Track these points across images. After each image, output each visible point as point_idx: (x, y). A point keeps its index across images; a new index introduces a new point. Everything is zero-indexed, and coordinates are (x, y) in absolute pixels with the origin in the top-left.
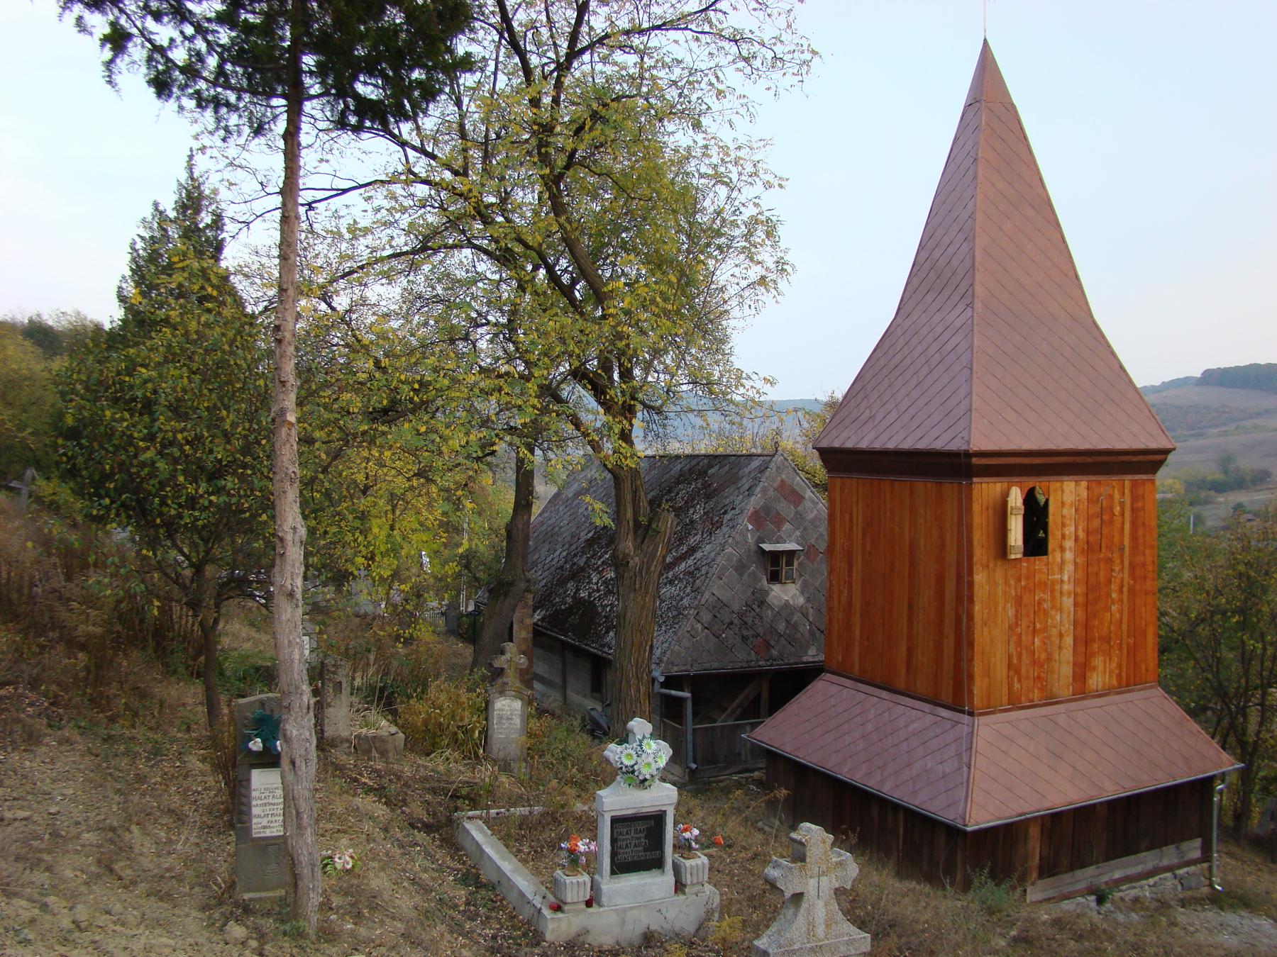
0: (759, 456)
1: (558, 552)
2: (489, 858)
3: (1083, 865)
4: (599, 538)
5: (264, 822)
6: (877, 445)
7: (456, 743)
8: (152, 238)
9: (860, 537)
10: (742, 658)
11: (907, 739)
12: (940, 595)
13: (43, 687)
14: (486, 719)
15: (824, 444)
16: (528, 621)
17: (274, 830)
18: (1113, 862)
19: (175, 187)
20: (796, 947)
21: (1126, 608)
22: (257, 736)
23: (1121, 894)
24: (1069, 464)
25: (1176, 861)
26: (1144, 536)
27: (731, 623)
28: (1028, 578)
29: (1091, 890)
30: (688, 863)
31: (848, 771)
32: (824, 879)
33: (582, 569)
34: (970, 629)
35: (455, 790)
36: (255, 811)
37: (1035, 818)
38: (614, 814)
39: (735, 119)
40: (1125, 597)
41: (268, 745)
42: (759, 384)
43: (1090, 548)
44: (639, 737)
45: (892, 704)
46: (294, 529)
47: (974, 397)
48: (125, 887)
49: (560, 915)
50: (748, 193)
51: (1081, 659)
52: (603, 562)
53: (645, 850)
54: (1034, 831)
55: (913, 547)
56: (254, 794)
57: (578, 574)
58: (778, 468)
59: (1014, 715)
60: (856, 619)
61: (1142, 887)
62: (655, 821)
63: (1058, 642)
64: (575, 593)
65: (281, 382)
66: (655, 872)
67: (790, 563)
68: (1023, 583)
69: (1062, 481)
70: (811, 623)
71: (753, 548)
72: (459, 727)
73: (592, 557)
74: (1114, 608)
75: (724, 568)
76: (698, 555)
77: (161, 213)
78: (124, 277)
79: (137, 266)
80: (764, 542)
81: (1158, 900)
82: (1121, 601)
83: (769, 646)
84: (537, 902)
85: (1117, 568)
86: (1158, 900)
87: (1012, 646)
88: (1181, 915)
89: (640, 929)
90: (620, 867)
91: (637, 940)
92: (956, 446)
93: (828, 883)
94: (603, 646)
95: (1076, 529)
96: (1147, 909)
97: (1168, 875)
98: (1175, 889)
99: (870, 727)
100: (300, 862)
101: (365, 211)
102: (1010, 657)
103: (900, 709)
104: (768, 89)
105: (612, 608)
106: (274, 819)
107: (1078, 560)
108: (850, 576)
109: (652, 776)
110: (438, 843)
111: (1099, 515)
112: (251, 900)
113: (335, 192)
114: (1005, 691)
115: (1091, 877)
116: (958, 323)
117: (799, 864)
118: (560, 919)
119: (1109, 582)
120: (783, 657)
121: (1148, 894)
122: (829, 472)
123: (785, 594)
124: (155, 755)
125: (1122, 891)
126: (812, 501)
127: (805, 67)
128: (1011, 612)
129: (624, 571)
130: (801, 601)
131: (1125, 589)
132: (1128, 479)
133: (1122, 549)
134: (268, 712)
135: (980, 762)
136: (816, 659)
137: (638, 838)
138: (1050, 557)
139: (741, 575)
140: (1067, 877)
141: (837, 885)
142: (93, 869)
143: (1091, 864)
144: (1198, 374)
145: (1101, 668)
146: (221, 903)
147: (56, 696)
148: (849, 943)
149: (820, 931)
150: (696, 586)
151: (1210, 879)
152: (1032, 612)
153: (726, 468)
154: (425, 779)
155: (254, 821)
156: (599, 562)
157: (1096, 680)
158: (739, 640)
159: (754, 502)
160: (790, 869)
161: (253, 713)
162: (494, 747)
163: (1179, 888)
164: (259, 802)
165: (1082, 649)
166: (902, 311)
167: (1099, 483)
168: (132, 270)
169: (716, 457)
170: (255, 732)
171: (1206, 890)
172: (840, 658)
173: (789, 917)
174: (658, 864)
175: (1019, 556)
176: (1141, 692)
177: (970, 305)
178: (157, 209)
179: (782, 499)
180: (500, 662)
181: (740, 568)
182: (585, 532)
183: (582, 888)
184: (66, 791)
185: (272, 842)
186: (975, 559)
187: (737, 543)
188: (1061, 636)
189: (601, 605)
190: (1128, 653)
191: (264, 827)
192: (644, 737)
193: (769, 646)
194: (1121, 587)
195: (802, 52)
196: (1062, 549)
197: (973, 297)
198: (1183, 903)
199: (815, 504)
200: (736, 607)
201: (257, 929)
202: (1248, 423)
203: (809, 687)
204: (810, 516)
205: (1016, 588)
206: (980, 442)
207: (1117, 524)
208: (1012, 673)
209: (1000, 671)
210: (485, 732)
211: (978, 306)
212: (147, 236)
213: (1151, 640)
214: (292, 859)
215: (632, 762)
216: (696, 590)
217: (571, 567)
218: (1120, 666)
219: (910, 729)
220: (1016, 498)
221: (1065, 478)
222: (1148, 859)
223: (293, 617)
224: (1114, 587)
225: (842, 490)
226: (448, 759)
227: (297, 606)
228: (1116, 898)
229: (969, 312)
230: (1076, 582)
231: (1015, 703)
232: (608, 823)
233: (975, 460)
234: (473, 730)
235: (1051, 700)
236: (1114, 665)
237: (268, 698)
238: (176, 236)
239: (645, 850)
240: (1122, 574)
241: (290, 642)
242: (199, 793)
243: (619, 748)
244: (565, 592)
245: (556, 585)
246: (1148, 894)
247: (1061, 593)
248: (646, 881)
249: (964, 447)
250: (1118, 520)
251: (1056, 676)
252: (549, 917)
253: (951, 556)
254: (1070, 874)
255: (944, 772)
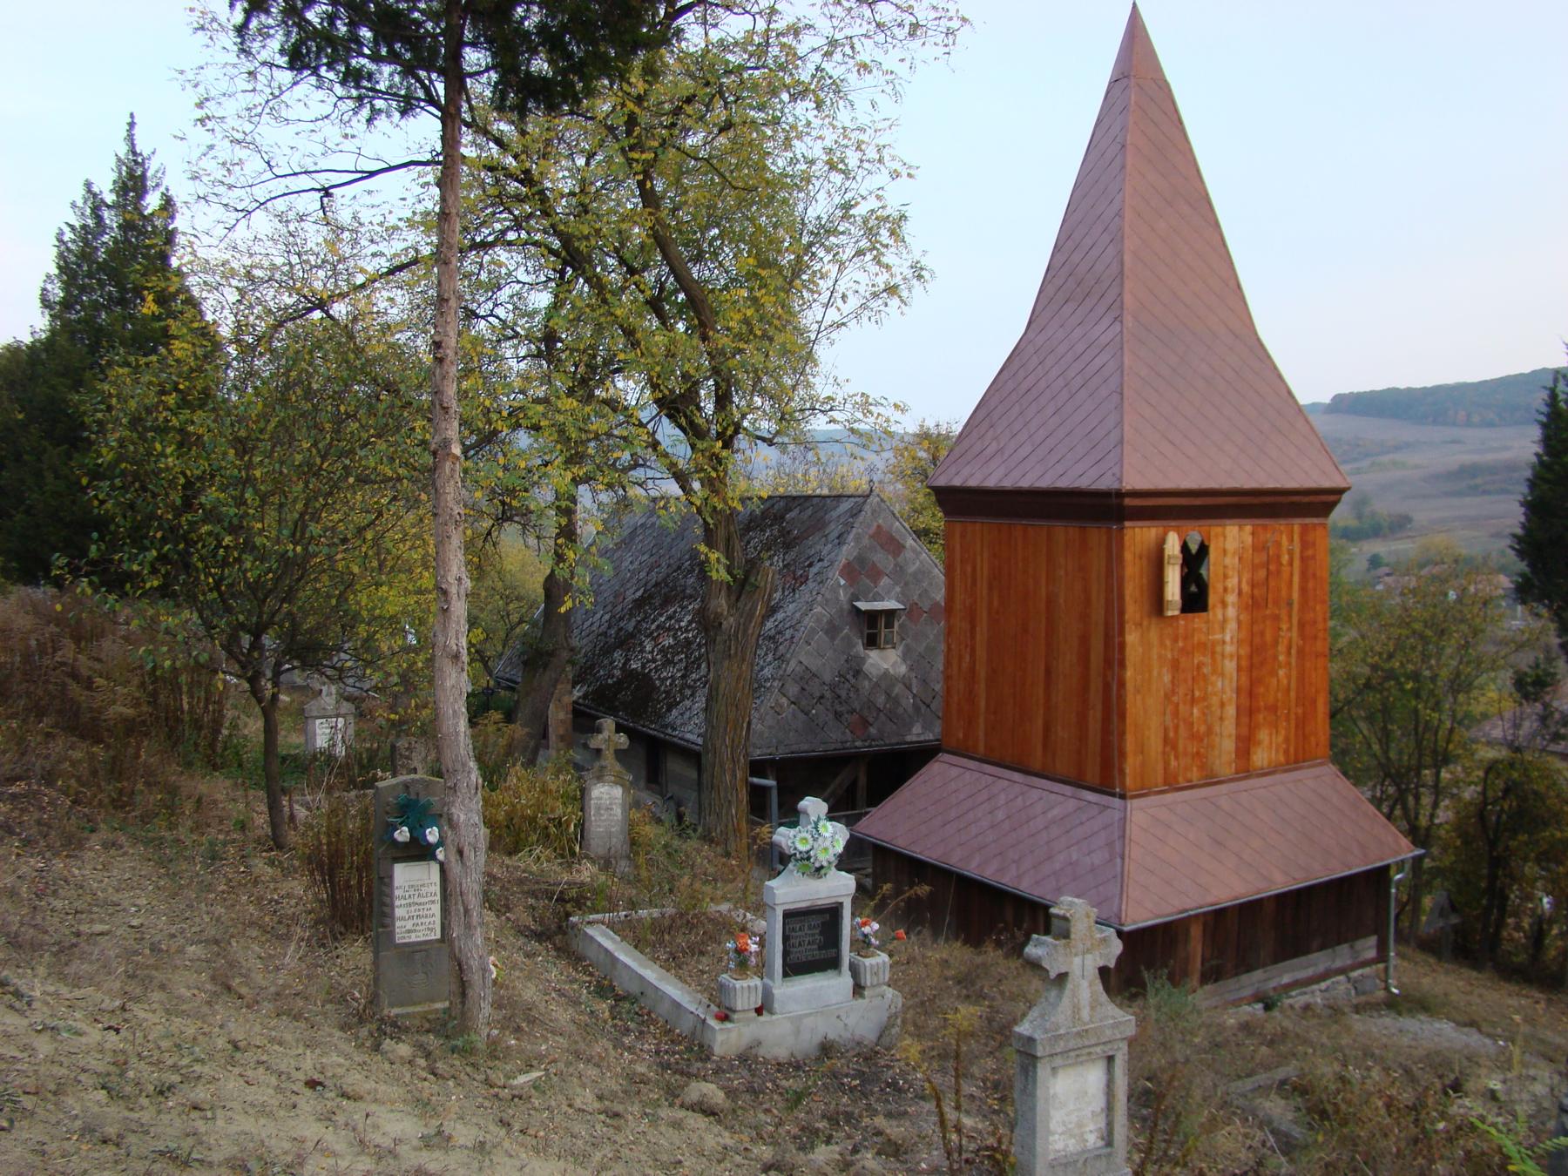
0: (849, 497)
1: (598, 616)
2: (626, 965)
3: (1250, 969)
4: (651, 597)
5: (409, 925)
6: (1008, 484)
7: (546, 837)
8: (84, 227)
9: (985, 592)
10: (836, 738)
11: (1046, 828)
12: (1084, 659)
13: (60, 783)
14: (582, 810)
15: (941, 482)
16: (568, 700)
17: (421, 934)
18: (1281, 965)
19: (113, 163)
20: (1062, 1031)
21: (1294, 673)
22: (402, 824)
23: (1290, 1001)
24: (1227, 506)
25: (1349, 962)
26: (1315, 590)
27: (822, 697)
28: (1185, 638)
29: (1258, 998)
30: (868, 962)
31: (974, 868)
32: (1089, 957)
33: (632, 636)
34: (1121, 698)
35: (561, 892)
36: (399, 912)
37: (1197, 916)
38: (787, 907)
39: (879, 98)
40: (1293, 661)
41: (415, 835)
42: (888, 412)
43: (1254, 604)
44: (813, 818)
45: (1026, 788)
46: (459, 580)
47: (1126, 428)
48: (248, 1007)
49: (728, 1025)
50: (865, 184)
51: (1244, 731)
52: (658, 627)
53: (820, 948)
54: (1196, 931)
55: (1050, 602)
56: (397, 893)
57: (626, 641)
58: (874, 511)
59: (1169, 797)
60: (981, 688)
61: (1313, 992)
62: (832, 914)
63: (1219, 712)
64: (624, 664)
65: (444, 408)
66: (830, 973)
67: (889, 625)
68: (1181, 644)
69: (1225, 525)
70: (914, 696)
71: (846, 607)
72: (549, 820)
73: (643, 620)
74: (1281, 673)
75: (813, 632)
76: (780, 616)
77: (95, 195)
78: (49, 276)
79: (65, 262)
80: (858, 600)
81: (1330, 1007)
82: (1289, 664)
83: (866, 723)
84: (701, 1013)
85: (1284, 627)
86: (1330, 1007)
87: (1168, 718)
88: (1358, 1023)
89: (818, 1039)
90: (793, 968)
91: (814, 1053)
92: (1105, 484)
93: (1093, 962)
94: (666, 726)
95: (1240, 582)
96: (1319, 1017)
97: (1341, 978)
98: (1348, 994)
99: (1000, 815)
100: (471, 967)
101: (404, 199)
102: (1166, 730)
103: (1035, 794)
104: (902, 60)
105: (673, 681)
106: (419, 921)
107: (1242, 617)
108: (973, 637)
109: (830, 863)
110: (553, 953)
111: (1265, 566)
112: (397, 1016)
113: (359, 175)
114: (1160, 767)
115: (1259, 982)
116: (1104, 339)
117: (1064, 941)
118: (729, 1030)
119: (1276, 643)
120: (883, 737)
121: (1319, 1000)
122: (946, 514)
123: (885, 661)
124: (213, 858)
125: (1291, 997)
126: (914, 550)
127: (950, 37)
128: (1167, 678)
129: (716, 635)
130: (903, 669)
131: (1293, 652)
132: (1297, 523)
133: (1290, 604)
134: (413, 797)
135: (1134, 852)
136: (922, 738)
137: (813, 935)
138: (1211, 613)
139: (833, 638)
140: (1231, 983)
141: (1101, 964)
142: (208, 986)
143: (1257, 969)
144: (1327, 400)
145: (1266, 742)
146: (361, 1021)
147: (77, 793)
148: (1115, 1026)
149: (1085, 1014)
150: (779, 654)
151: (1386, 982)
152: (1190, 677)
153: (809, 512)
154: (521, 882)
155: (398, 924)
156: (653, 627)
157: (1261, 757)
158: (831, 716)
159: (847, 552)
160: (1055, 946)
161: (396, 798)
162: (592, 842)
163: (1353, 992)
164: (403, 902)
165: (1245, 720)
166: (1033, 326)
167: (1265, 527)
168: (59, 267)
169: (795, 498)
170: (399, 820)
171: (1381, 994)
172: (961, 735)
173: (1051, 1000)
174: (833, 964)
175: (1177, 613)
176: (1313, 770)
177: (1118, 318)
178: (89, 191)
179: (878, 548)
180: (597, 741)
181: (832, 630)
182: (632, 591)
183: (753, 994)
184: (138, 902)
185: (418, 948)
186: (1127, 617)
187: (827, 601)
188: (1222, 705)
189: (659, 678)
190: (1297, 726)
191: (409, 931)
192: (819, 819)
193: (866, 723)
194: (1289, 648)
195: (951, 19)
196: (1224, 605)
197: (1122, 308)
198: (1357, 1009)
199: (918, 554)
200: (827, 677)
201: (420, 1046)
202: (1385, 459)
203: (923, 770)
204: (912, 569)
205: (1172, 650)
206: (1134, 480)
207: (1285, 575)
208: (1168, 749)
209: (1155, 744)
210: (581, 825)
211: (1128, 320)
212: (77, 225)
213: (1322, 708)
214: (459, 965)
215: (808, 847)
216: (780, 658)
217: (617, 633)
218: (1287, 740)
219: (1050, 815)
220: (1173, 545)
221: (1228, 522)
222: (1319, 961)
223: (458, 682)
224: (1282, 648)
225: (963, 536)
226: (539, 858)
227: (463, 670)
228: (1286, 1006)
229: (1117, 327)
230: (1240, 642)
231: (1172, 784)
232: (781, 918)
233: (1127, 501)
234: (568, 823)
235: (1211, 780)
236: (1281, 739)
237: (413, 780)
238: (115, 225)
239: (820, 948)
240: (1290, 633)
241: (455, 711)
242: (277, 903)
243: (792, 832)
244: (611, 663)
245: (599, 655)
246: (1319, 1000)
247: (1223, 655)
248: (820, 984)
249: (1116, 486)
250: (1286, 570)
251: (1216, 752)
252: (717, 1028)
253: (1098, 615)
254: (1236, 979)
255: (1093, 864)
